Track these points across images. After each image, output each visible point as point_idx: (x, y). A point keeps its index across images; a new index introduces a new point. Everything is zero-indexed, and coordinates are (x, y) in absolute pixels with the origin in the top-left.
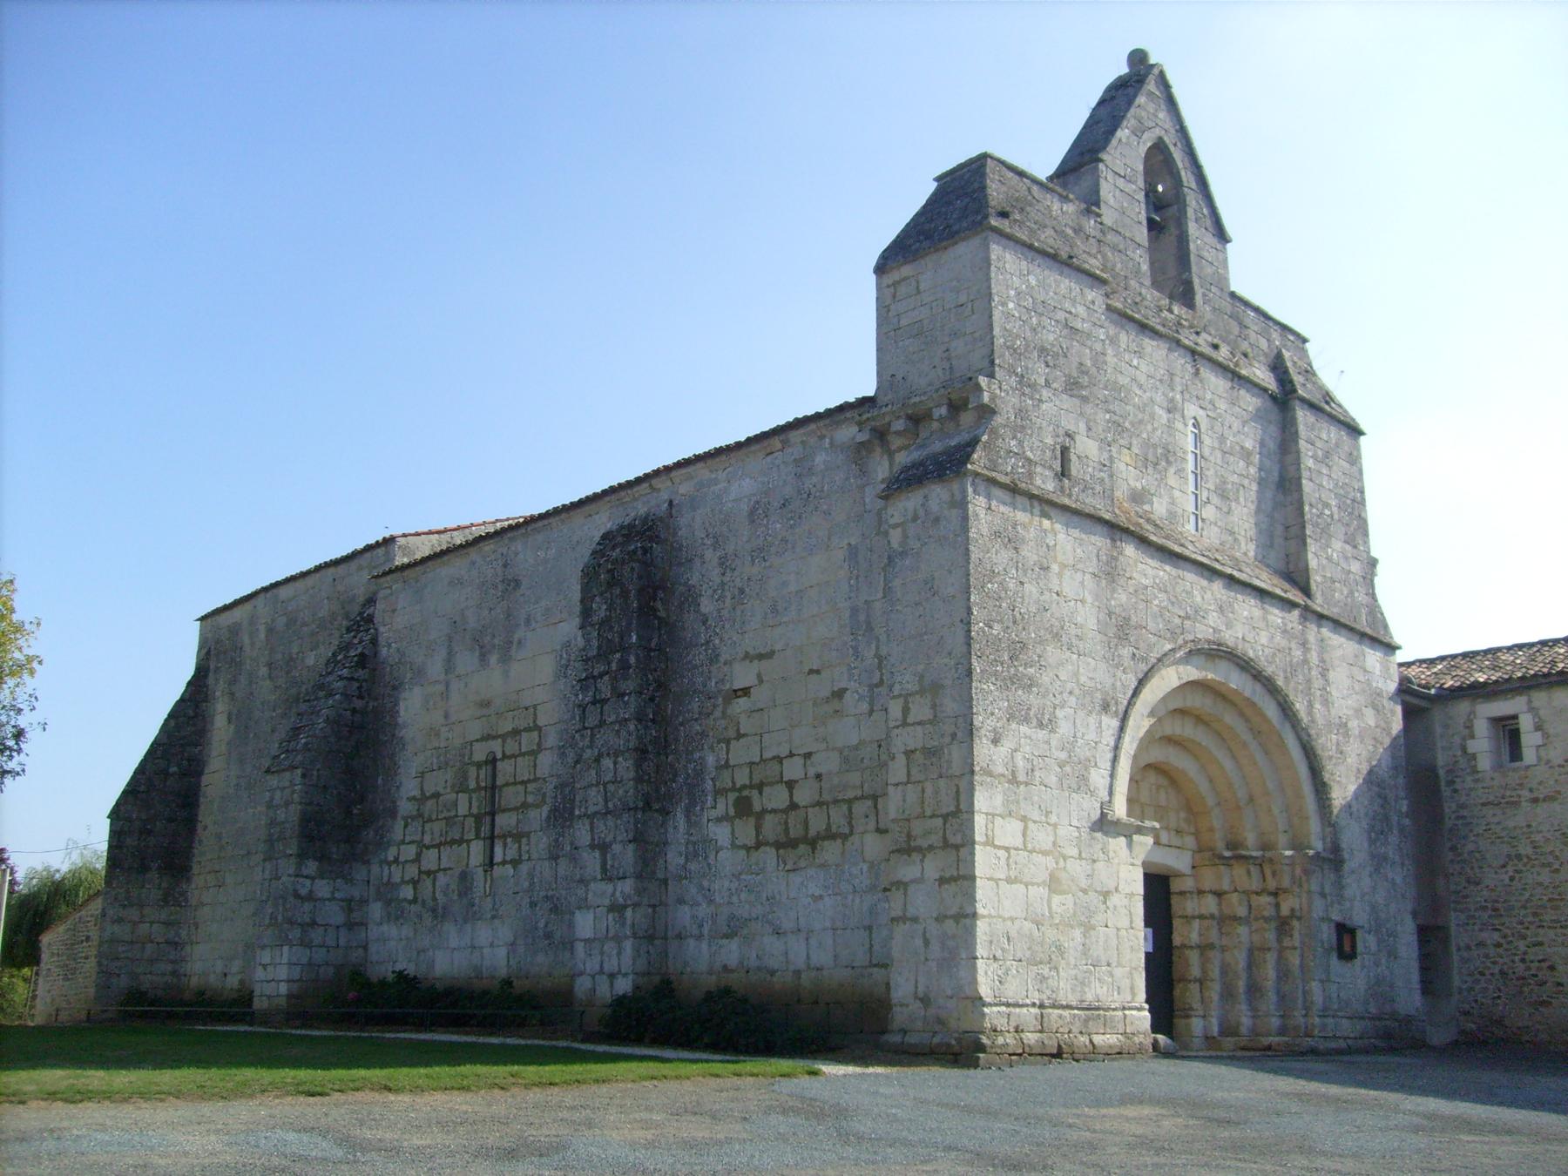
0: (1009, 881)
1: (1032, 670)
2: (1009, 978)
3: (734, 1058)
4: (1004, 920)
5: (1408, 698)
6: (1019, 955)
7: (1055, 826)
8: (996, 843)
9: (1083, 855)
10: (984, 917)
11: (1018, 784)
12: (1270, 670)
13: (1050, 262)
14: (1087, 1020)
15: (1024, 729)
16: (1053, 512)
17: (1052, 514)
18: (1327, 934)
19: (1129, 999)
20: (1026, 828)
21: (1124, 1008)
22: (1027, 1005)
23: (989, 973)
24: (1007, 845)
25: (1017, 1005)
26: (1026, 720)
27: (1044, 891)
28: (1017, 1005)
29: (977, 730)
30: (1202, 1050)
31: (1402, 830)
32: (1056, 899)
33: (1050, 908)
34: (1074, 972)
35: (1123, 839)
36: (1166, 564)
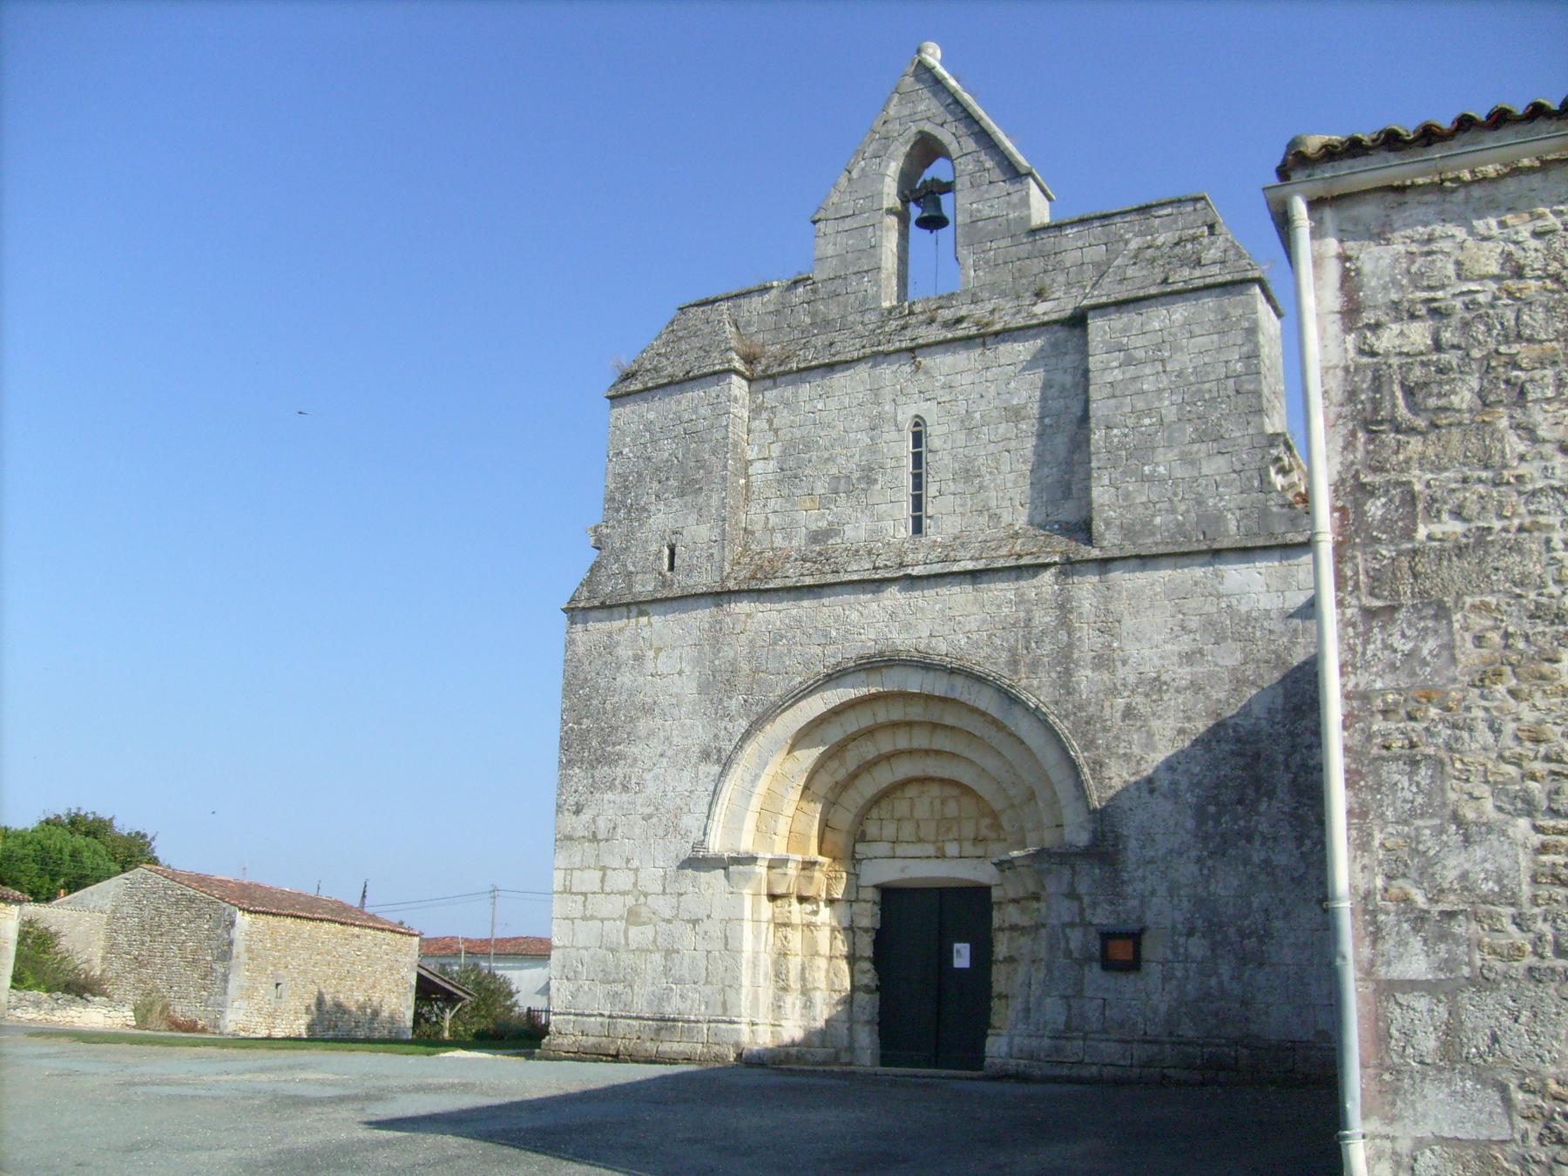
0: (584, 918)
1: (621, 747)
2: (581, 994)
3: (511, 965)
4: (578, 949)
6: (592, 976)
7: (637, 870)
8: (574, 890)
10: (557, 947)
11: (598, 841)
12: (987, 668)
13: (672, 388)
14: (659, 1030)
15: (609, 796)
17: (649, 611)
18: (1037, 286)
19: (719, 1013)
20: (604, 875)
23: (562, 990)
24: (584, 890)
25: (583, 1015)
26: (611, 788)
27: (621, 925)
28: (583, 1015)
32: (633, 930)
33: (626, 938)
34: (652, 989)
35: (722, 871)
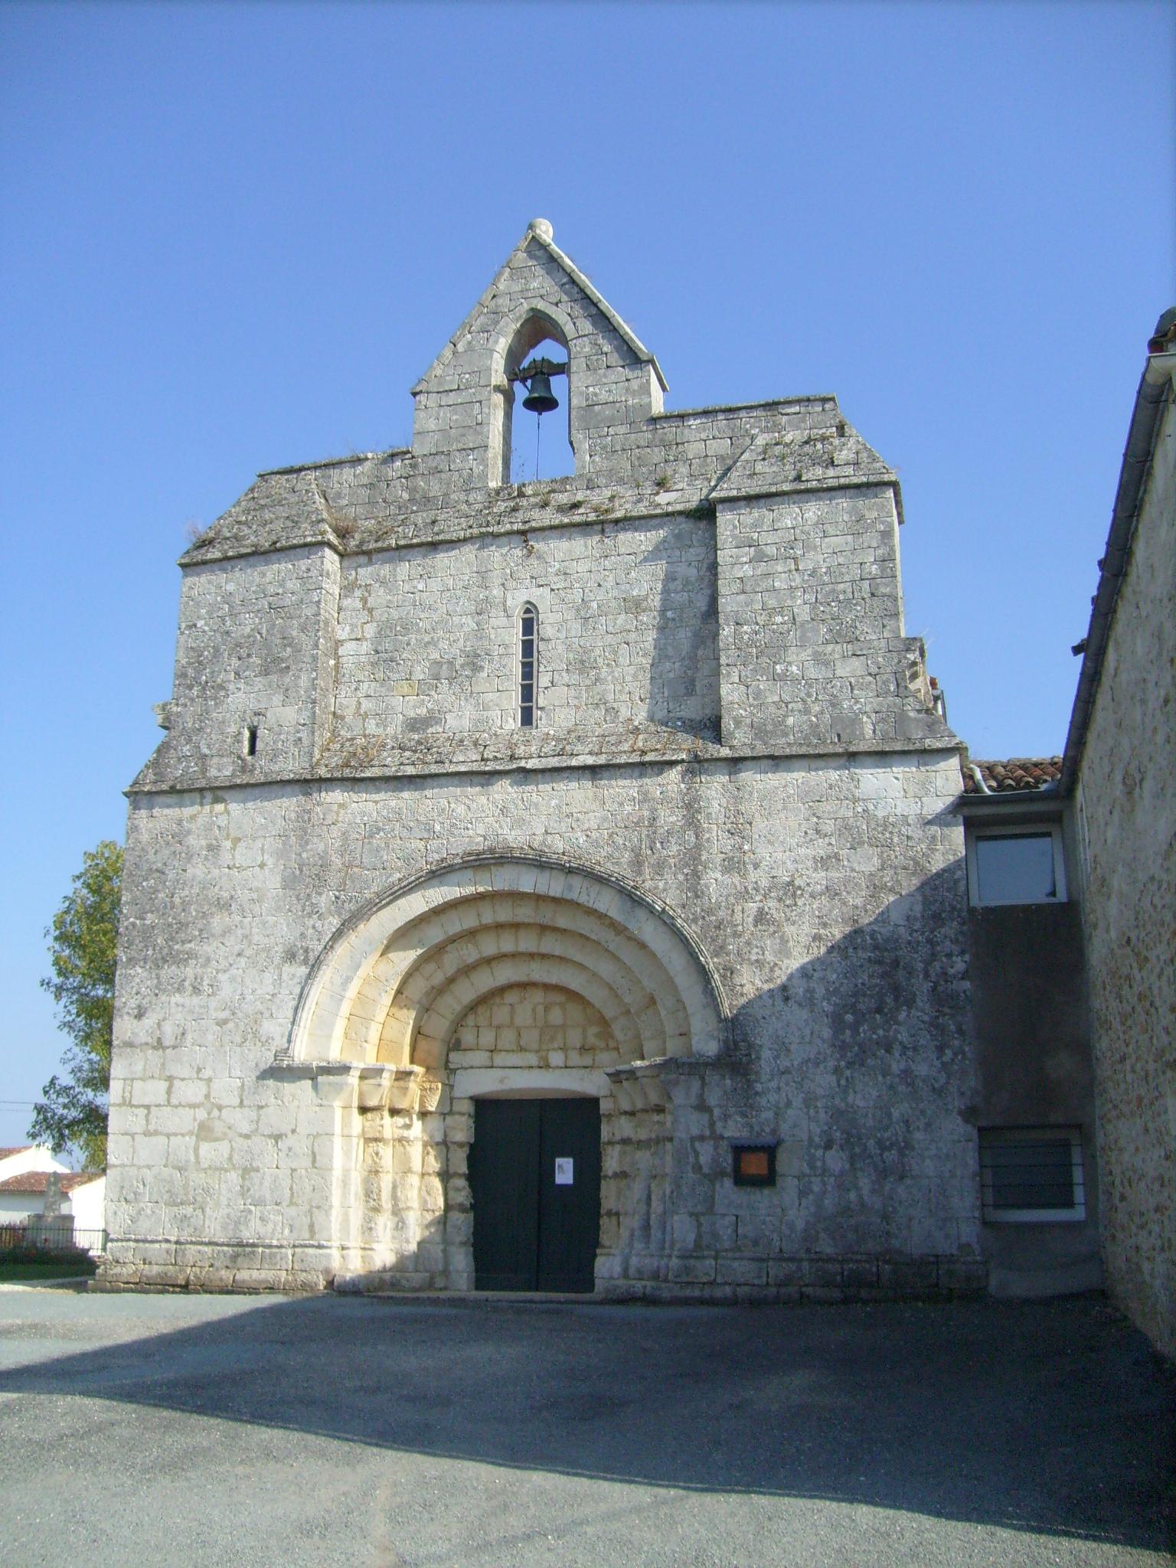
4: (139, 1168)
5: (966, 811)
7: (209, 1080)
8: (134, 1102)
9: (246, 1102)
10: (115, 1166)
15: (177, 998)
16: (227, 795)
21: (294, 1246)
22: (160, 1242)
23: (119, 1213)
26: (180, 989)
28: (145, 1241)
29: (119, 1010)
30: (814, 1285)
31: (942, 999)
33: (197, 1156)
36: (401, 791)
